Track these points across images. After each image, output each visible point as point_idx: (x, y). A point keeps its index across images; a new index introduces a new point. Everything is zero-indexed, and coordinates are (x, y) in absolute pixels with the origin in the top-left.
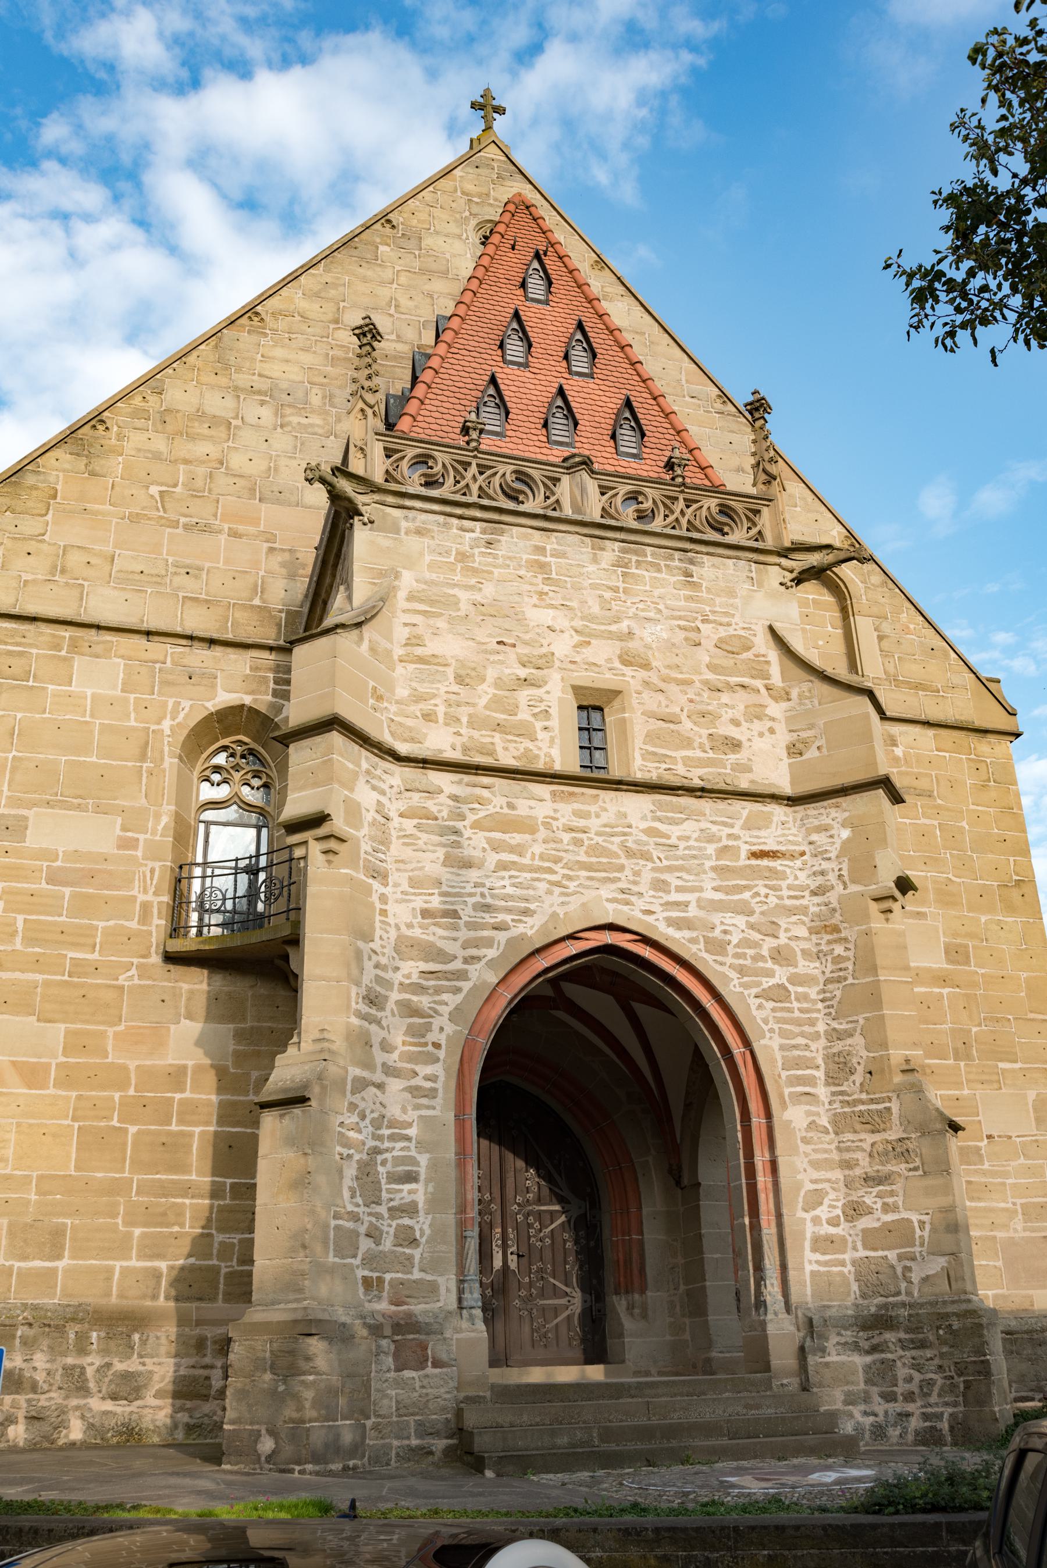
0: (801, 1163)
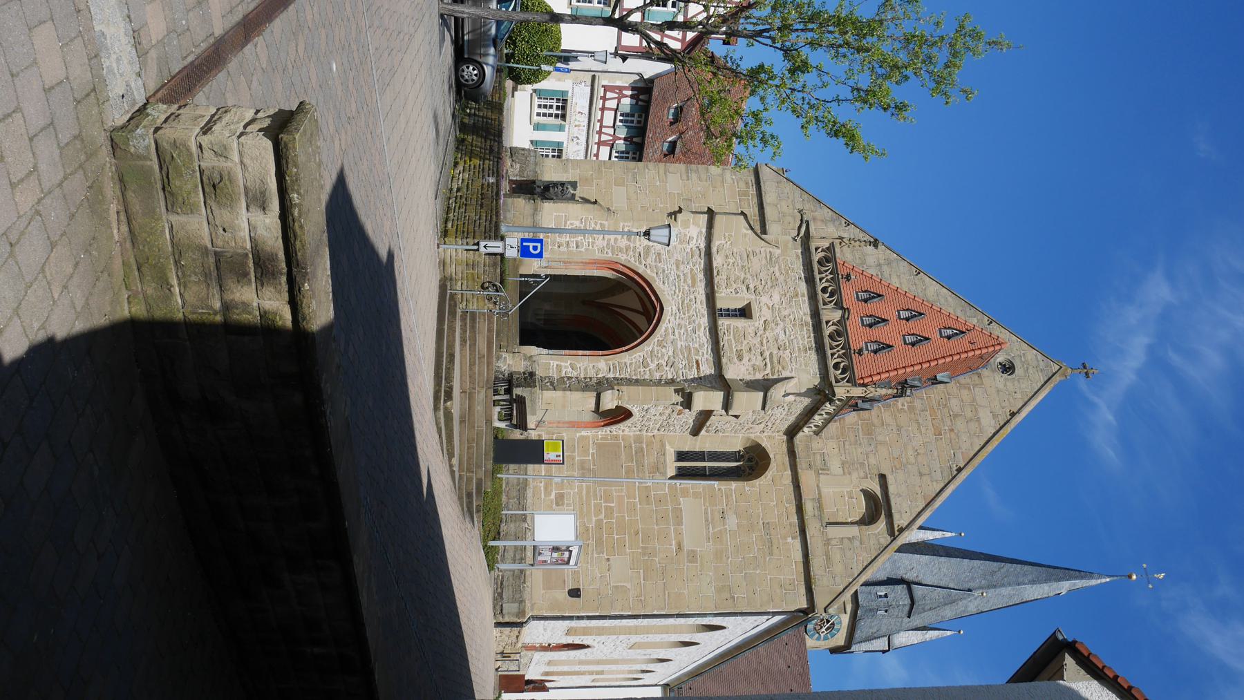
0: (586, 364)
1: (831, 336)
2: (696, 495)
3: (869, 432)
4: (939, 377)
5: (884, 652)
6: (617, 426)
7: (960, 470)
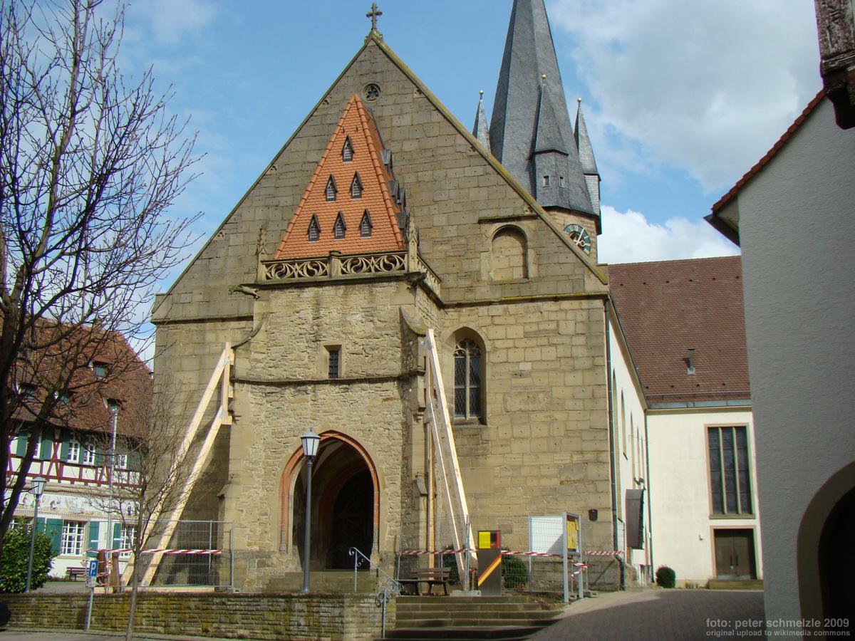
1: (357, 269)
5: (599, 180)
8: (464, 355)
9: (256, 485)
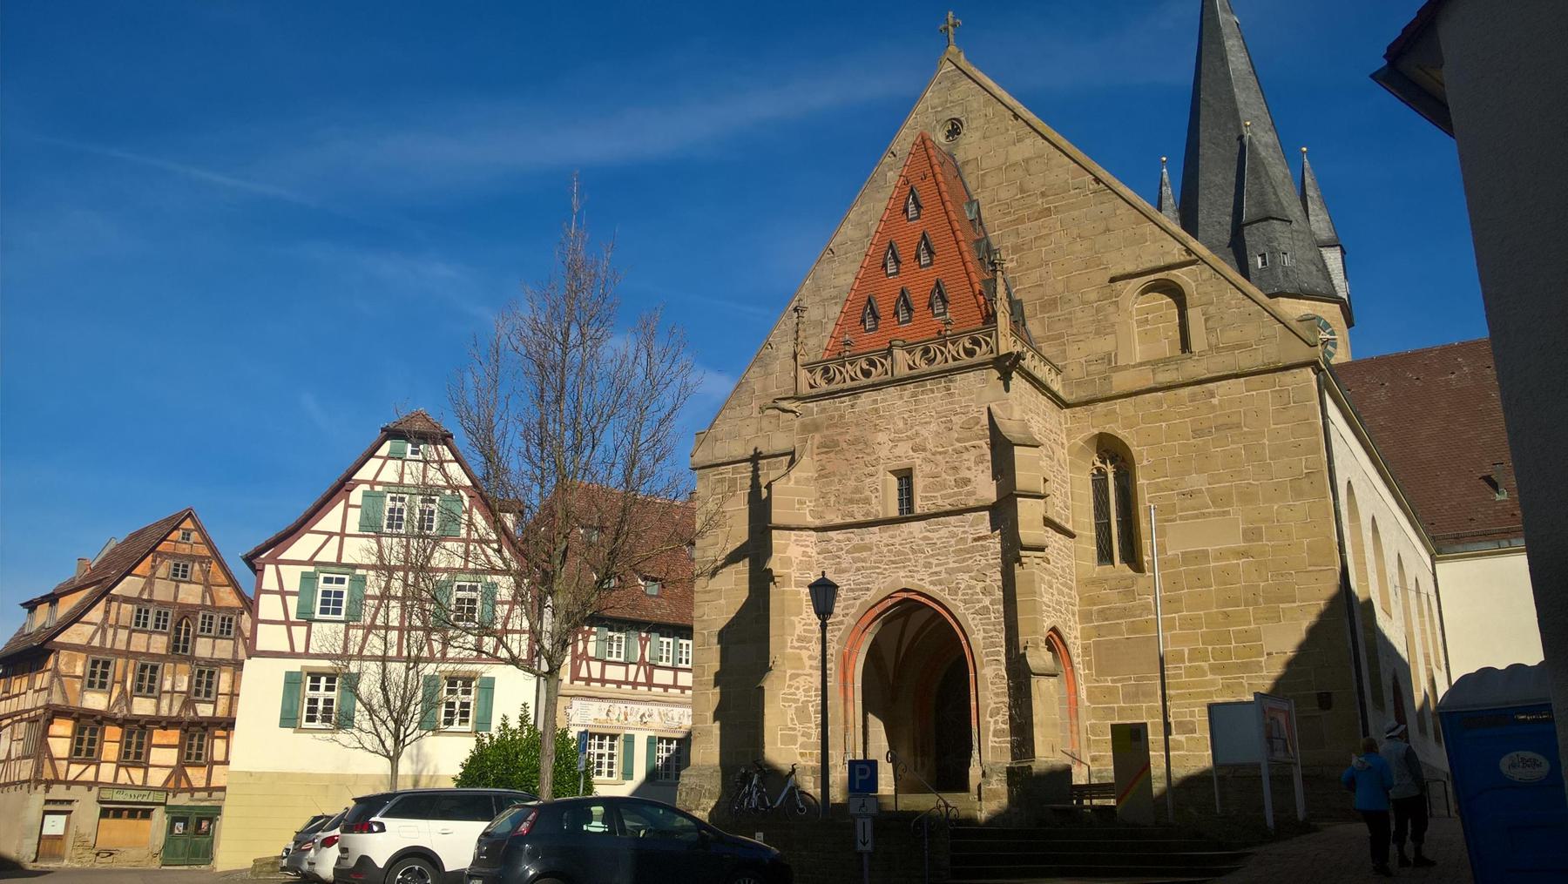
0: (989, 695)
2: (1161, 533)
3: (1050, 304)
4: (969, 216)
5: (1343, 252)
6: (1071, 647)
7: (1097, 180)
8: (1106, 475)
9: (808, 671)
